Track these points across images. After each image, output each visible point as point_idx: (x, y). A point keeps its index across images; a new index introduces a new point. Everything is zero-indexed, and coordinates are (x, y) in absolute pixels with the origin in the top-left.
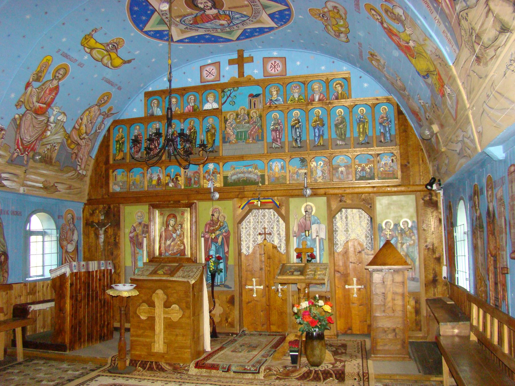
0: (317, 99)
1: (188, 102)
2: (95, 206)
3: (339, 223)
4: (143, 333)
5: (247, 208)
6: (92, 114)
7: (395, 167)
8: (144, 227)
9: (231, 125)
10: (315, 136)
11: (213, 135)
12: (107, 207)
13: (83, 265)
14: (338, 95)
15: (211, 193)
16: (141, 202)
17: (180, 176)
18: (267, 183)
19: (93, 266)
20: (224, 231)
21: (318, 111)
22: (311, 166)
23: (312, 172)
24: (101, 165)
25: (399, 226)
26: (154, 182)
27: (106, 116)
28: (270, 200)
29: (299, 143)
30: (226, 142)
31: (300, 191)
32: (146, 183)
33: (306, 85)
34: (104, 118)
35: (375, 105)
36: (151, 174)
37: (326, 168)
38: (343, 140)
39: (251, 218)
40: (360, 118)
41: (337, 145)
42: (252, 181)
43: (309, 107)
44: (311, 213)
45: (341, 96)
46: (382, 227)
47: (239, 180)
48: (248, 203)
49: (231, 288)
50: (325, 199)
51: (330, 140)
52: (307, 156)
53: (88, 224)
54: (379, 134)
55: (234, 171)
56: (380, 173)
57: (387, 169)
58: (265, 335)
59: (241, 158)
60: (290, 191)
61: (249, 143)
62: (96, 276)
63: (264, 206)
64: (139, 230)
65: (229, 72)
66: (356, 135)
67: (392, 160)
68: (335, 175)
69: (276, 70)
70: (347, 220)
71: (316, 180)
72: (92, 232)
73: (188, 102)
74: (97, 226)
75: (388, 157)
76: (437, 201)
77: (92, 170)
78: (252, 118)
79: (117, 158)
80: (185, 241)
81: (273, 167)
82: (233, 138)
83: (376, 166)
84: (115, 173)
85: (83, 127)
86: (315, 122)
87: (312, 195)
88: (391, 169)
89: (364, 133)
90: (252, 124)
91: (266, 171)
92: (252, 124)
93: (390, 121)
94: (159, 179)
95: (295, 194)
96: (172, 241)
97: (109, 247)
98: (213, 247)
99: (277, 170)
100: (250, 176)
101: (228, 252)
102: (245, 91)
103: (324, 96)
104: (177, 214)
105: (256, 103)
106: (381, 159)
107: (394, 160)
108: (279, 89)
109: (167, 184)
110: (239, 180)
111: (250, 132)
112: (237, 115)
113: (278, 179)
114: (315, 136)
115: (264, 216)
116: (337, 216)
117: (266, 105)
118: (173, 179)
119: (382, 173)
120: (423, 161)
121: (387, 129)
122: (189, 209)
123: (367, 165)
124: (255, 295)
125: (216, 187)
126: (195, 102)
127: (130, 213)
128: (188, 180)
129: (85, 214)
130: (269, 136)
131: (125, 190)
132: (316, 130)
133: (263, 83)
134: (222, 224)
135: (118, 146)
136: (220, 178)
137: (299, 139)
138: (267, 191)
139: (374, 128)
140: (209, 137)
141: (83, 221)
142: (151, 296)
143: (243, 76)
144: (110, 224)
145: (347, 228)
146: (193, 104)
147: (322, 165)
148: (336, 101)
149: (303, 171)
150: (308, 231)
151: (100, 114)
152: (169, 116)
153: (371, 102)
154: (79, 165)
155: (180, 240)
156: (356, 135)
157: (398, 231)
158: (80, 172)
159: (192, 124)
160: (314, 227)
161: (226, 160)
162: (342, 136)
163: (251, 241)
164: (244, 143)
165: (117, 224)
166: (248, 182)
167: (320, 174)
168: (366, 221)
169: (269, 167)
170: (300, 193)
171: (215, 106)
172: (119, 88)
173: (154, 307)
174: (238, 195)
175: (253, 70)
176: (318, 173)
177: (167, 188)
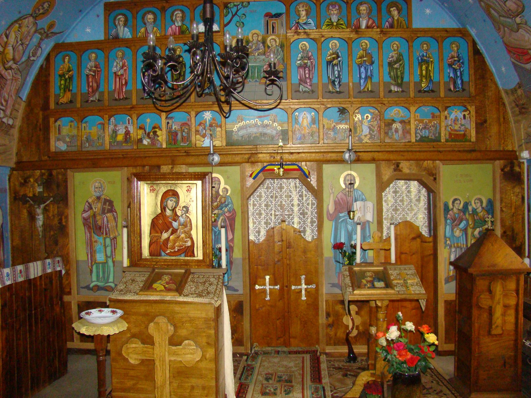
0: (363, 26)
1: (172, 20)
2: (28, 173)
4: (134, 385)
6: (24, 29)
7: (468, 126)
8: (105, 204)
13: (21, 271)
14: (393, 22)
15: (210, 154)
16: (97, 167)
19: (36, 269)
20: (226, 210)
22: (354, 120)
24: (36, 111)
25: (471, 205)
26: (120, 138)
28: (296, 167)
29: (337, 86)
31: (339, 154)
32: (107, 139)
34: (41, 39)
37: (375, 123)
38: (399, 85)
40: (423, 56)
41: (390, 91)
45: (398, 23)
49: (237, 290)
50: (373, 166)
53: (18, 198)
54: (448, 80)
57: (456, 127)
58: (284, 352)
62: (41, 285)
64: (97, 207)
66: (418, 79)
67: (464, 116)
71: (360, 140)
72: (25, 211)
74: (32, 202)
75: (458, 112)
76: (520, 173)
77: (23, 119)
78: (269, 47)
80: (193, 233)
81: (300, 120)
84: (58, 123)
85: (10, 49)
86: (360, 58)
89: (428, 77)
93: (463, 63)
94: (127, 133)
96: (172, 234)
97: (52, 233)
99: (305, 123)
101: (232, 240)
103: (374, 22)
104: (178, 190)
105: (276, 26)
106: (449, 114)
107: (467, 116)
109: (140, 141)
115: (281, 188)
118: (149, 133)
120: (504, 118)
122: (199, 183)
124: (268, 298)
126: (183, 20)
127: (83, 183)
128: (172, 136)
129: (12, 185)
132: (362, 69)
134: (223, 200)
135: (63, 82)
141: (10, 195)
142: (147, 327)
144: (52, 199)
146: (180, 24)
148: (391, 30)
149: (343, 126)
151: (36, 32)
152: (208, 16)
154: (3, 110)
155: (185, 232)
156: (418, 79)
157: (469, 212)
158: (5, 120)
160: (357, 206)
164: (257, 84)
165: (63, 199)
169: (294, 119)
170: (339, 158)
173: (153, 344)
174: (249, 158)
176: (364, 130)
177: (140, 147)
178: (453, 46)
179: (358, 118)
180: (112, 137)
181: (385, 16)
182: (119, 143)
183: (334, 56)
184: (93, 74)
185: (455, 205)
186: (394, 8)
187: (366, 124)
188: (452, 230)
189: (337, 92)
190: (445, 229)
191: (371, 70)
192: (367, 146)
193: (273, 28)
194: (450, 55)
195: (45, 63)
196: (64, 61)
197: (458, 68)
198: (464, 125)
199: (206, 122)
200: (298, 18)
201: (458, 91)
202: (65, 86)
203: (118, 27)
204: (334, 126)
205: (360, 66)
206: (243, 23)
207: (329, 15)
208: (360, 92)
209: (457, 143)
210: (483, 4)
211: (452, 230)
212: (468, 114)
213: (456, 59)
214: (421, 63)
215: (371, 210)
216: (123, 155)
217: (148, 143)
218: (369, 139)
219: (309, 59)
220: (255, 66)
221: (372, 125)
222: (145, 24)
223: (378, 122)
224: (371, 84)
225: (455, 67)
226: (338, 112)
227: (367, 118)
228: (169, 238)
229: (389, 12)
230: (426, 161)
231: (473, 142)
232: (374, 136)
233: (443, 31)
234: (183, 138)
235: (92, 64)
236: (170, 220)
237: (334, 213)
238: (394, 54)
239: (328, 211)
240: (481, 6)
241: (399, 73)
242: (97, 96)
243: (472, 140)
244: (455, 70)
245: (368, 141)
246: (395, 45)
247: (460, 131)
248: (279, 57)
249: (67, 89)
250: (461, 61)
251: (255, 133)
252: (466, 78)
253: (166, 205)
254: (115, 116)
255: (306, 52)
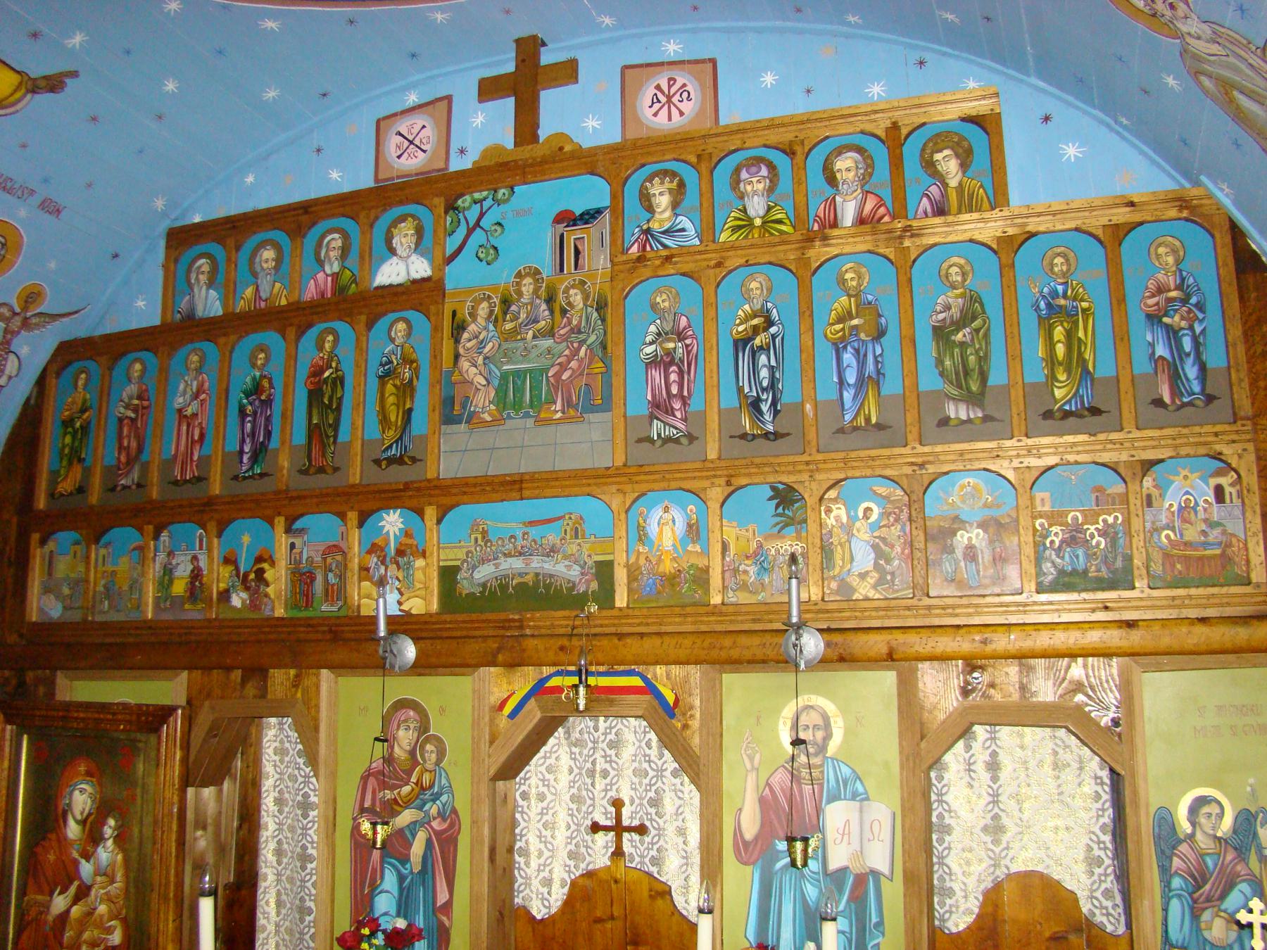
3: (960, 790)
5: (534, 713)
9: (482, 345)
10: (842, 382)
11: (407, 389)
12: (14, 682)
14: (944, 195)
15: (378, 640)
16: (120, 668)
17: (273, 564)
18: (621, 600)
20: (434, 811)
21: (850, 262)
23: (826, 551)
26: (179, 588)
27: (17, 321)
28: (636, 681)
29: (768, 417)
30: (457, 421)
31: (768, 638)
32: (150, 593)
33: (800, 157)
35: (1119, 233)
36: (171, 554)
37: (896, 531)
38: (974, 399)
39: (564, 753)
40: (1054, 294)
41: (944, 422)
42: (559, 591)
43: (811, 253)
44: (822, 749)
46: (1173, 827)
47: (503, 587)
48: (540, 689)
50: (887, 679)
51: (912, 400)
52: (805, 477)
54: (1149, 369)
55: (494, 544)
56: (1157, 556)
57: (1191, 534)
59: (514, 486)
60: (727, 642)
61: (548, 422)
63: (603, 700)
65: (485, 128)
67: (1219, 492)
68: (939, 563)
69: (674, 112)
70: (995, 779)
71: (846, 589)
73: (317, 254)
79: (60, 489)
81: (653, 529)
82: (483, 402)
83: (1136, 524)
84: (51, 545)
86: (840, 320)
87: (825, 662)
88: (1214, 534)
89: (1077, 364)
90: (565, 338)
91: (622, 545)
92: (565, 338)
93: (1200, 306)
94: (196, 575)
95: (747, 654)
96: (76, 900)
98: (390, 881)
99: (667, 543)
100: (548, 566)
101: (447, 908)
102: (542, 199)
103: (881, 203)
105: (584, 248)
106: (1161, 487)
107: (1228, 489)
108: (682, 185)
109: (225, 596)
110: (503, 587)
111: (558, 375)
112: (506, 302)
113: (672, 580)
114: (842, 382)
116: (948, 757)
117: (625, 251)
118: (246, 575)
119: (1167, 556)
121: (1187, 344)
123: (1091, 517)
125: (408, 614)
128: (302, 578)
130: (637, 390)
131: (76, 616)
132: (848, 357)
133: (609, 163)
134: (427, 778)
135: (68, 440)
136: (425, 571)
137: (767, 397)
138: (621, 636)
139: (1121, 337)
140: (392, 399)
143: (535, 138)
145: (996, 817)
146: (336, 268)
147: (874, 517)
148: (938, 220)
149: (788, 545)
150: (805, 840)
153: (1104, 221)
159: (327, 346)
160: (836, 815)
161: (445, 495)
162: (969, 380)
163: (563, 854)
164: (530, 422)
166: (542, 594)
167: (864, 558)
168: (1089, 788)
169: (633, 528)
171: (420, 268)
172: (51, 208)
175: (581, 116)
176: (858, 557)
178: (1161, 250)
179: (837, 518)
180: (161, 583)
181: (917, 181)
182: (177, 602)
183: (755, 322)
184: (133, 415)
185: (1202, 820)
186: (946, 152)
187: (863, 534)
188: (1195, 916)
189: (766, 435)
190: (1165, 910)
191: (875, 357)
192: (865, 610)
193: (577, 252)
194: (1151, 285)
195: (35, 393)
196: (76, 386)
197: (1183, 324)
198: (1218, 524)
199: (388, 543)
200: (648, 215)
201: (1190, 404)
202: (72, 448)
203: (196, 290)
204: (760, 546)
205: (838, 348)
206: (496, 249)
207: (742, 198)
208: (841, 431)
209: (1193, 591)
210: (1206, 81)
211: (1195, 916)
212: (1232, 485)
213: (1173, 294)
214: (1049, 318)
215: (886, 834)
216: (180, 635)
217: (243, 602)
218: (874, 587)
219: (681, 336)
220: (525, 371)
221: (883, 539)
222: (255, 275)
223: (903, 529)
224: (878, 405)
225: (1175, 320)
226: (771, 499)
227: (866, 517)
228: (68, 911)
229: (930, 166)
230: (1080, 660)
231: (1258, 585)
232: (893, 574)
233: (1117, 205)
234: (327, 590)
235: (133, 389)
236: (75, 855)
237: (756, 838)
238: (955, 300)
239: (738, 830)
240: (1206, 92)
241: (972, 358)
242: (135, 475)
243: (1254, 577)
244: (1172, 334)
245: (871, 594)
246: (954, 270)
247: (1205, 545)
248: (592, 338)
249: (75, 456)
250: (1193, 300)
251: (521, 575)
252: (1216, 357)
253: (69, 805)
254: (172, 528)
255: (670, 318)
